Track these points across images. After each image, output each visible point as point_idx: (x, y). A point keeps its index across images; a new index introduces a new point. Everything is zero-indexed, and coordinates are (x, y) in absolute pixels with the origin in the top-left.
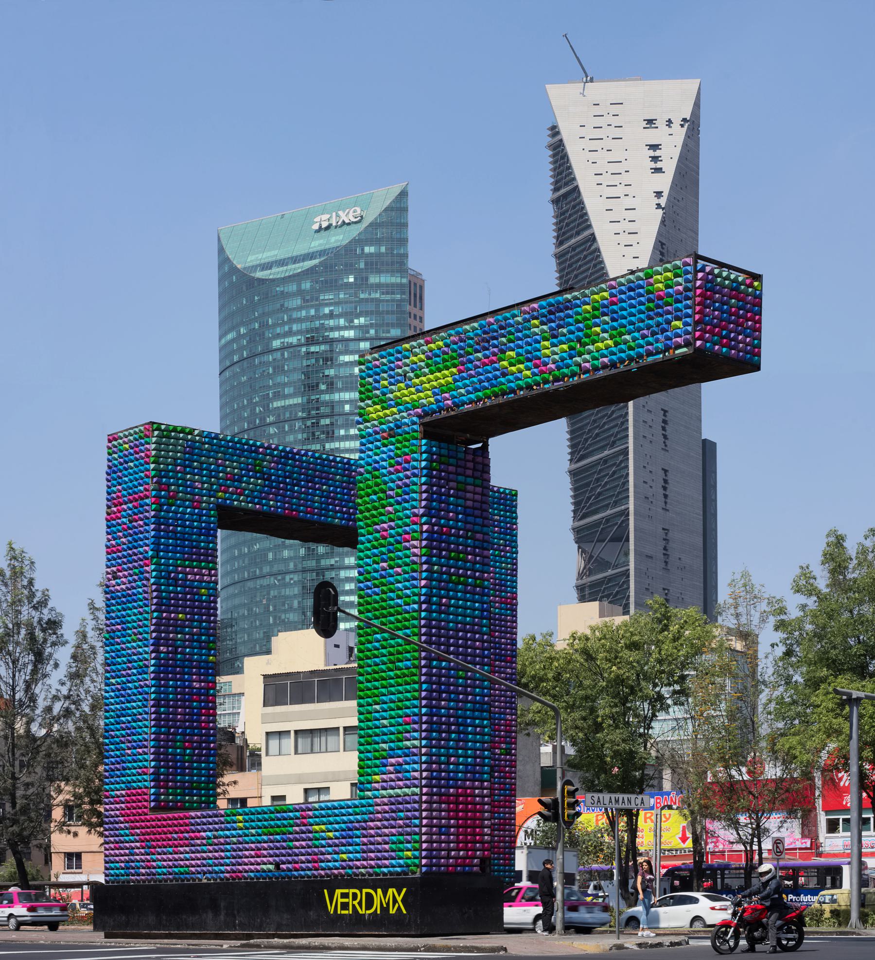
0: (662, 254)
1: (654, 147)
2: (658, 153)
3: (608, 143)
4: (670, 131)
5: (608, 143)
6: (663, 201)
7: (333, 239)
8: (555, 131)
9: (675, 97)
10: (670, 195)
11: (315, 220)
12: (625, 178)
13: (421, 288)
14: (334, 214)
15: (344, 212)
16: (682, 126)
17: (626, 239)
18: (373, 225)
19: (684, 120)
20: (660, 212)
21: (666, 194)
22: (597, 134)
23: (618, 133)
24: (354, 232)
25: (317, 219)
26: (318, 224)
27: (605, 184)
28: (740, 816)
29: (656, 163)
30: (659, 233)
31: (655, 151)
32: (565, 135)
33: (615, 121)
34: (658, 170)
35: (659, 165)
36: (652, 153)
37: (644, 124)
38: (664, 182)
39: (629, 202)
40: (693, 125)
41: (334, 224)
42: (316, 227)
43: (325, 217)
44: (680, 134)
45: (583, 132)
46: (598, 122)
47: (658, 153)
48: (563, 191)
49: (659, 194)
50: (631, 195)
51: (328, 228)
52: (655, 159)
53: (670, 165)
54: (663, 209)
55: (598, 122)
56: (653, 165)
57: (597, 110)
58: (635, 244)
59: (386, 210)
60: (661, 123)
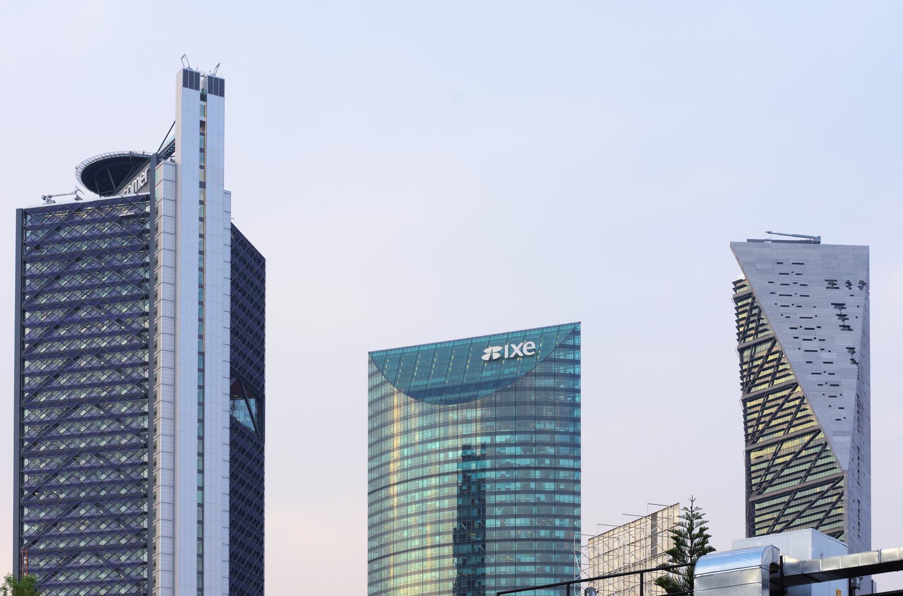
2: (843, 312)
12: (818, 333)
16: (861, 288)
23: (803, 290)
25: (488, 351)
27: (801, 337)
33: (801, 280)
35: (847, 323)
36: (838, 311)
39: (825, 356)
41: (506, 356)
45: (772, 288)
49: (851, 350)
52: (842, 317)
57: (782, 268)
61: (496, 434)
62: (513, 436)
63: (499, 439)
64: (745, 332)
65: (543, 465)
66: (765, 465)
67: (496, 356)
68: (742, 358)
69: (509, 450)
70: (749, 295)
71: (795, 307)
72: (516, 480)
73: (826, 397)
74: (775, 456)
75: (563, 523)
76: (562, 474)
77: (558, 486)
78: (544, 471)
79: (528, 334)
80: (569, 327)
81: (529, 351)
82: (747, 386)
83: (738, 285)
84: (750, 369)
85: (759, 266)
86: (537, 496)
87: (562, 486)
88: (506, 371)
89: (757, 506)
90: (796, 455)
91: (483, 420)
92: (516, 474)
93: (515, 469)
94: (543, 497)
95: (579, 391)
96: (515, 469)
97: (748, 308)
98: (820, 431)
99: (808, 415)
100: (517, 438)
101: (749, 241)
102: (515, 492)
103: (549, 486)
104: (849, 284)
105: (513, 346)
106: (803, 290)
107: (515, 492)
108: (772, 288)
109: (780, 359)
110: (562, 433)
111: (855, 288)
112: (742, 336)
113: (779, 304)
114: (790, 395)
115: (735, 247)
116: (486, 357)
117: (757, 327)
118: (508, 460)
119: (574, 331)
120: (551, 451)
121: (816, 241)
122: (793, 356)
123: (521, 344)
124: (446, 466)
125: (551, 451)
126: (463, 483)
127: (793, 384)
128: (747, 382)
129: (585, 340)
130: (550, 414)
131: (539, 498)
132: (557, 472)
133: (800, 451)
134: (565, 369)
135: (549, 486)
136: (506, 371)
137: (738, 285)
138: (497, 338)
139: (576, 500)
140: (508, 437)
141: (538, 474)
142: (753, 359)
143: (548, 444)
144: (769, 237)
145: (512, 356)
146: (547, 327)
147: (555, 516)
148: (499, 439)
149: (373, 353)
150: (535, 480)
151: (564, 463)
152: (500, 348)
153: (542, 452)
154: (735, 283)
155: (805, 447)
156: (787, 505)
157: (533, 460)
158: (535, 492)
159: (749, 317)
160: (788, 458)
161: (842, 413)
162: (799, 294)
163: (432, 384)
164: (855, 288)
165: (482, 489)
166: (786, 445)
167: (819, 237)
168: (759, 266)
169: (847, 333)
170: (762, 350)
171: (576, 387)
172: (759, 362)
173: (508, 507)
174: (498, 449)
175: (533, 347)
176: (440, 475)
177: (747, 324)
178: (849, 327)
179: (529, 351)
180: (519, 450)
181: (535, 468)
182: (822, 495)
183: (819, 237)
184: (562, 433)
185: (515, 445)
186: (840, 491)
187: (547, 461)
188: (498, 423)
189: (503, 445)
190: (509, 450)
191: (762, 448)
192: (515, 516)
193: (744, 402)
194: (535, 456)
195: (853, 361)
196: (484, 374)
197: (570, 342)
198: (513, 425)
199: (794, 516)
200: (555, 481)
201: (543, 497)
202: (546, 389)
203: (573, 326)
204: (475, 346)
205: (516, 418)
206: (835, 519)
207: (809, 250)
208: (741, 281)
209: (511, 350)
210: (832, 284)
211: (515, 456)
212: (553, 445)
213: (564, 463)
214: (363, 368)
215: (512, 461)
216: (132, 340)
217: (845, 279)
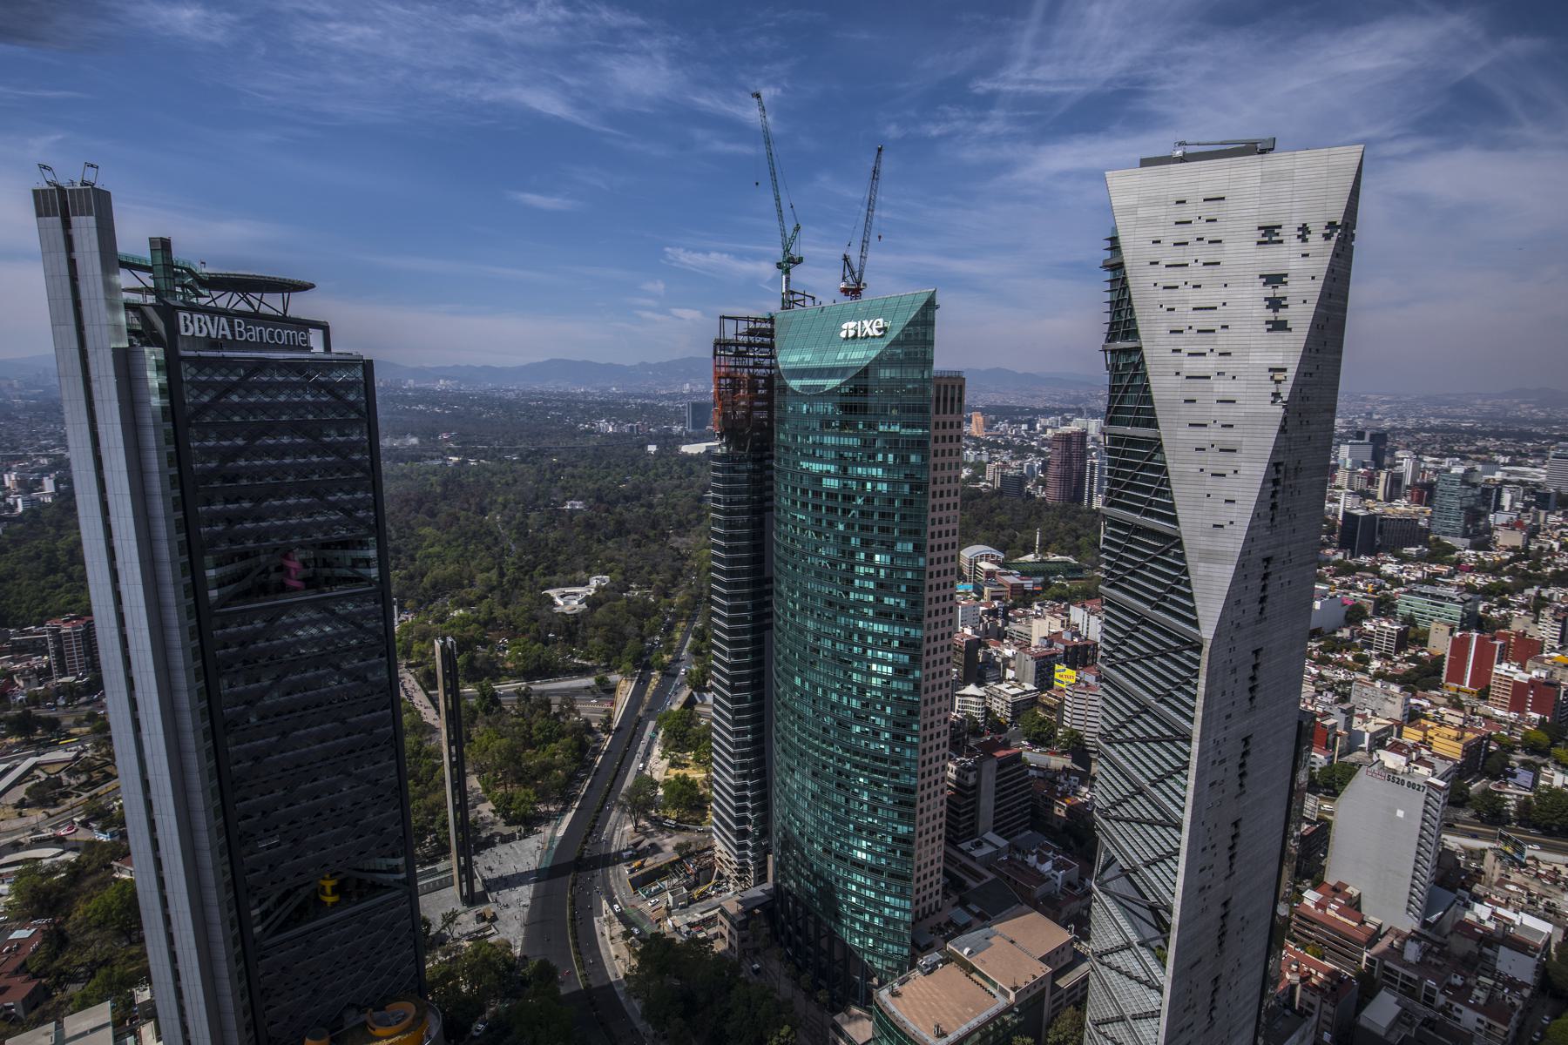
1: (1274, 279)
2: (1281, 291)
3: (1196, 273)
4: (1305, 248)
6: (1285, 391)
7: (841, 356)
8: (1114, 244)
12: (1222, 340)
13: (961, 388)
16: (1327, 237)
17: (1214, 461)
19: (1331, 225)
20: (1279, 410)
21: (1291, 374)
22: (1178, 255)
23: (1211, 253)
25: (844, 326)
27: (1186, 350)
29: (1276, 311)
30: (1276, 451)
32: (1128, 256)
33: (1210, 232)
34: (1279, 326)
36: (1269, 291)
37: (1258, 235)
38: (1288, 352)
39: (1222, 387)
40: (1343, 233)
42: (843, 334)
43: (852, 324)
44: (1321, 251)
46: (1186, 233)
47: (1281, 291)
50: (1229, 375)
53: (1301, 315)
55: (1186, 233)
56: (1270, 315)
58: (1230, 473)
59: (910, 324)
60: (1289, 233)
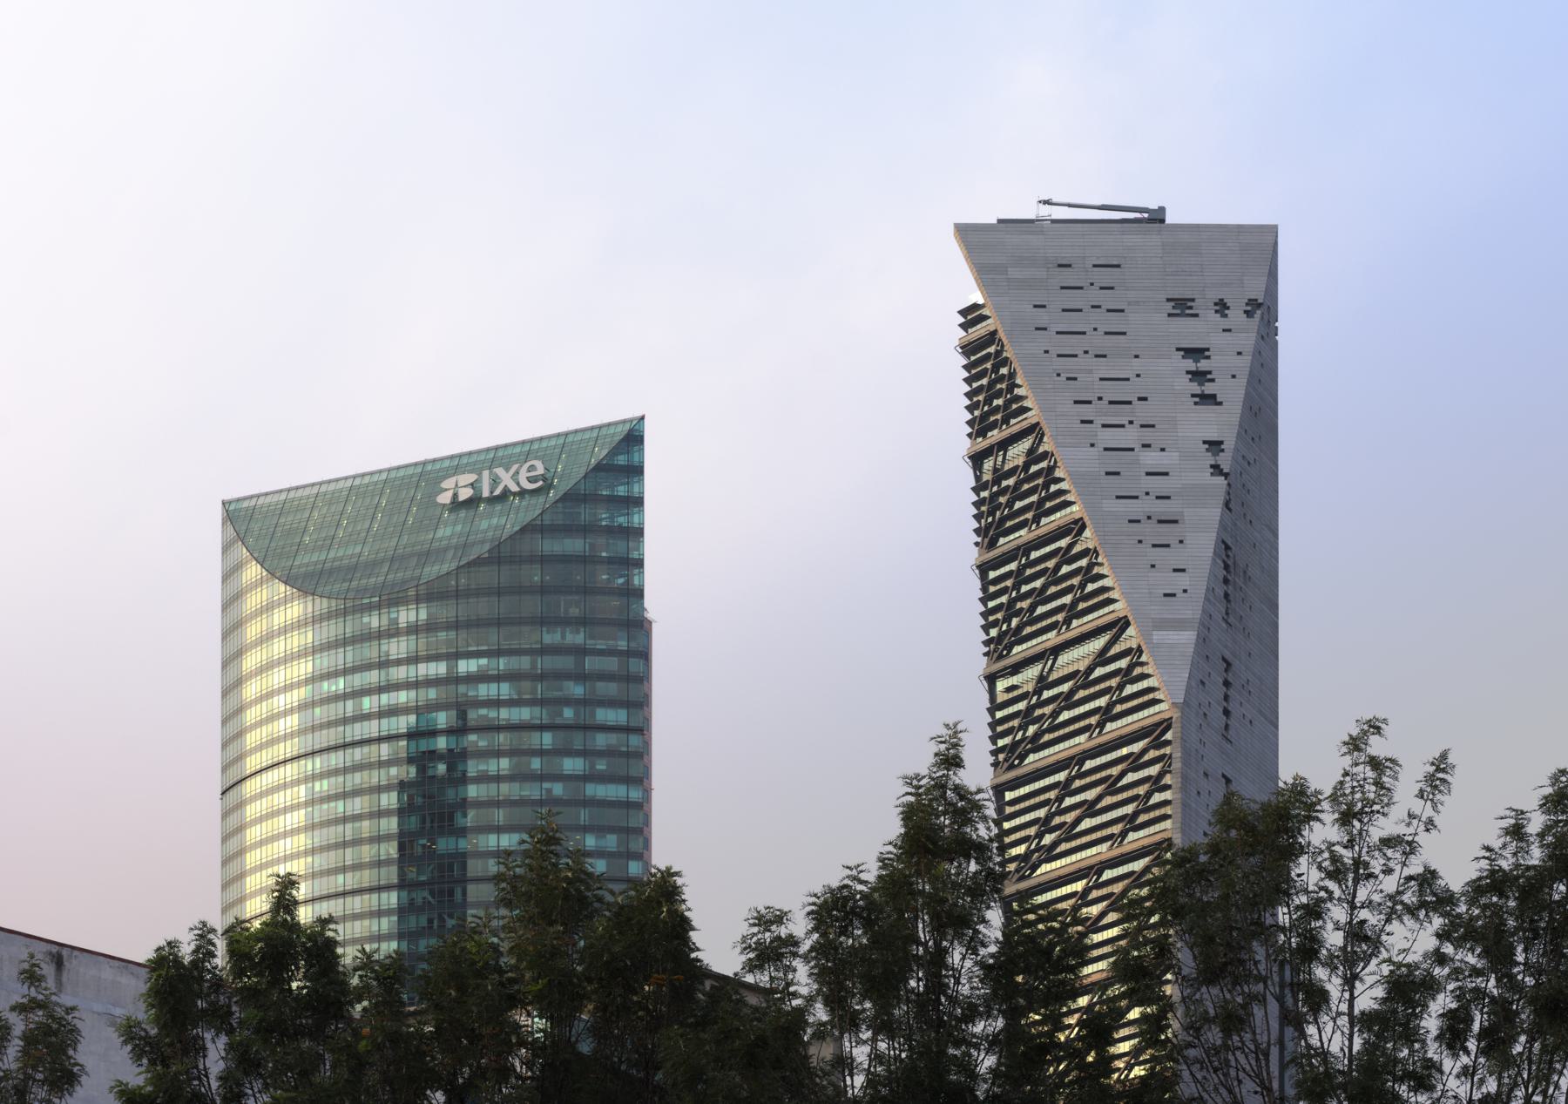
0: (1226, 567)
2: (1203, 365)
4: (1225, 323)
5: (1099, 342)
9: (981, 301)
10: (1236, 450)
11: (444, 485)
12: (1141, 412)
14: (486, 474)
15: (507, 470)
16: (1249, 314)
18: (570, 498)
19: (1251, 302)
21: (1229, 445)
23: (1115, 322)
24: (527, 512)
25: (448, 483)
26: (449, 494)
27: (1099, 421)
28: (357, 1016)
31: (1197, 361)
33: (1107, 299)
35: (1209, 388)
36: (1190, 365)
39: (1151, 459)
41: (486, 494)
45: (1042, 317)
48: (995, 436)
49: (1214, 446)
51: (472, 502)
52: (1199, 376)
53: (1233, 392)
54: (1226, 475)
57: (1069, 277)
61: (457, 656)
62: (494, 661)
63: (466, 666)
64: (984, 416)
65: (558, 721)
66: (1021, 706)
67: (464, 494)
68: (978, 478)
69: (485, 691)
70: (992, 337)
71: (1090, 359)
72: (498, 754)
73: (1146, 547)
74: (1043, 683)
75: (602, 843)
76: (602, 740)
77: (592, 766)
78: (561, 734)
79: (536, 446)
80: (619, 429)
81: (531, 480)
82: (989, 534)
83: (971, 316)
84: (994, 496)
85: (1014, 273)
86: (546, 785)
87: (601, 766)
88: (484, 524)
89: (1009, 796)
90: (1082, 678)
91: (431, 627)
92: (503, 739)
93: (499, 729)
94: (558, 789)
95: (639, 563)
96: (499, 729)
97: (985, 359)
98: (1127, 624)
99: (1105, 589)
100: (503, 663)
101: (1000, 221)
102: (498, 779)
103: (572, 765)
104: (1222, 307)
105: (500, 471)
106: (1115, 322)
107: (498, 779)
108: (1042, 317)
109: (1051, 469)
110: (601, 653)
111: (1236, 315)
112: (980, 427)
113: (1054, 351)
114: (1071, 546)
115: (967, 234)
116: (445, 498)
117: (1008, 403)
118: (483, 712)
119: (632, 437)
120: (577, 690)
121: (1157, 217)
122: (1073, 463)
123: (515, 467)
124: (357, 726)
125: (577, 690)
126: (845, 999)
127: (1076, 522)
128: (988, 526)
129: (653, 456)
130: (574, 612)
131: (549, 791)
132: (588, 734)
133: (1090, 670)
134: (612, 518)
135: (572, 765)
136: (484, 524)
137: (971, 316)
138: (474, 458)
139: (635, 795)
140: (483, 661)
141: (547, 739)
142: (999, 475)
143: (568, 676)
144: (1046, 211)
145: (497, 492)
146: (576, 432)
147: (586, 829)
148: (466, 666)
149: (230, 502)
150: (541, 753)
151: (606, 715)
152: (472, 478)
153: (557, 694)
154: (963, 312)
155: (1102, 658)
156: (1066, 789)
157: (537, 710)
158: (541, 777)
159: (992, 384)
160: (1065, 687)
161: (1183, 581)
162: (1102, 330)
163: (334, 560)
164: (1236, 315)
165: (430, 773)
166: (1064, 658)
167: (1162, 210)
168: (1014, 273)
169: (1208, 411)
170: (1017, 454)
171: (635, 555)
172: (1011, 482)
173: (483, 811)
174: (462, 689)
175: (540, 470)
176: (345, 746)
177: (988, 401)
178: (1214, 396)
179: (531, 480)
180: (505, 690)
181: (542, 728)
182: (1135, 762)
183: (1162, 210)
184: (601, 653)
185: (498, 678)
186: (1167, 750)
187: (568, 713)
188: (463, 634)
189: (472, 679)
190: (485, 691)
191: (1016, 669)
192: (499, 830)
193: (983, 569)
194: (542, 702)
195: (1217, 469)
196: (440, 533)
197: (621, 460)
198: (493, 637)
199: (1077, 812)
200: (584, 753)
201: (558, 789)
202: (566, 559)
203: (627, 427)
204: (427, 475)
205: (499, 623)
206: (1157, 813)
207: (1151, 239)
208: (975, 307)
209: (495, 481)
210: (1182, 307)
211: (497, 703)
212: (582, 677)
213: (606, 715)
214: (212, 530)
215: (493, 714)
216: (590, 980)
217: (1214, 295)
